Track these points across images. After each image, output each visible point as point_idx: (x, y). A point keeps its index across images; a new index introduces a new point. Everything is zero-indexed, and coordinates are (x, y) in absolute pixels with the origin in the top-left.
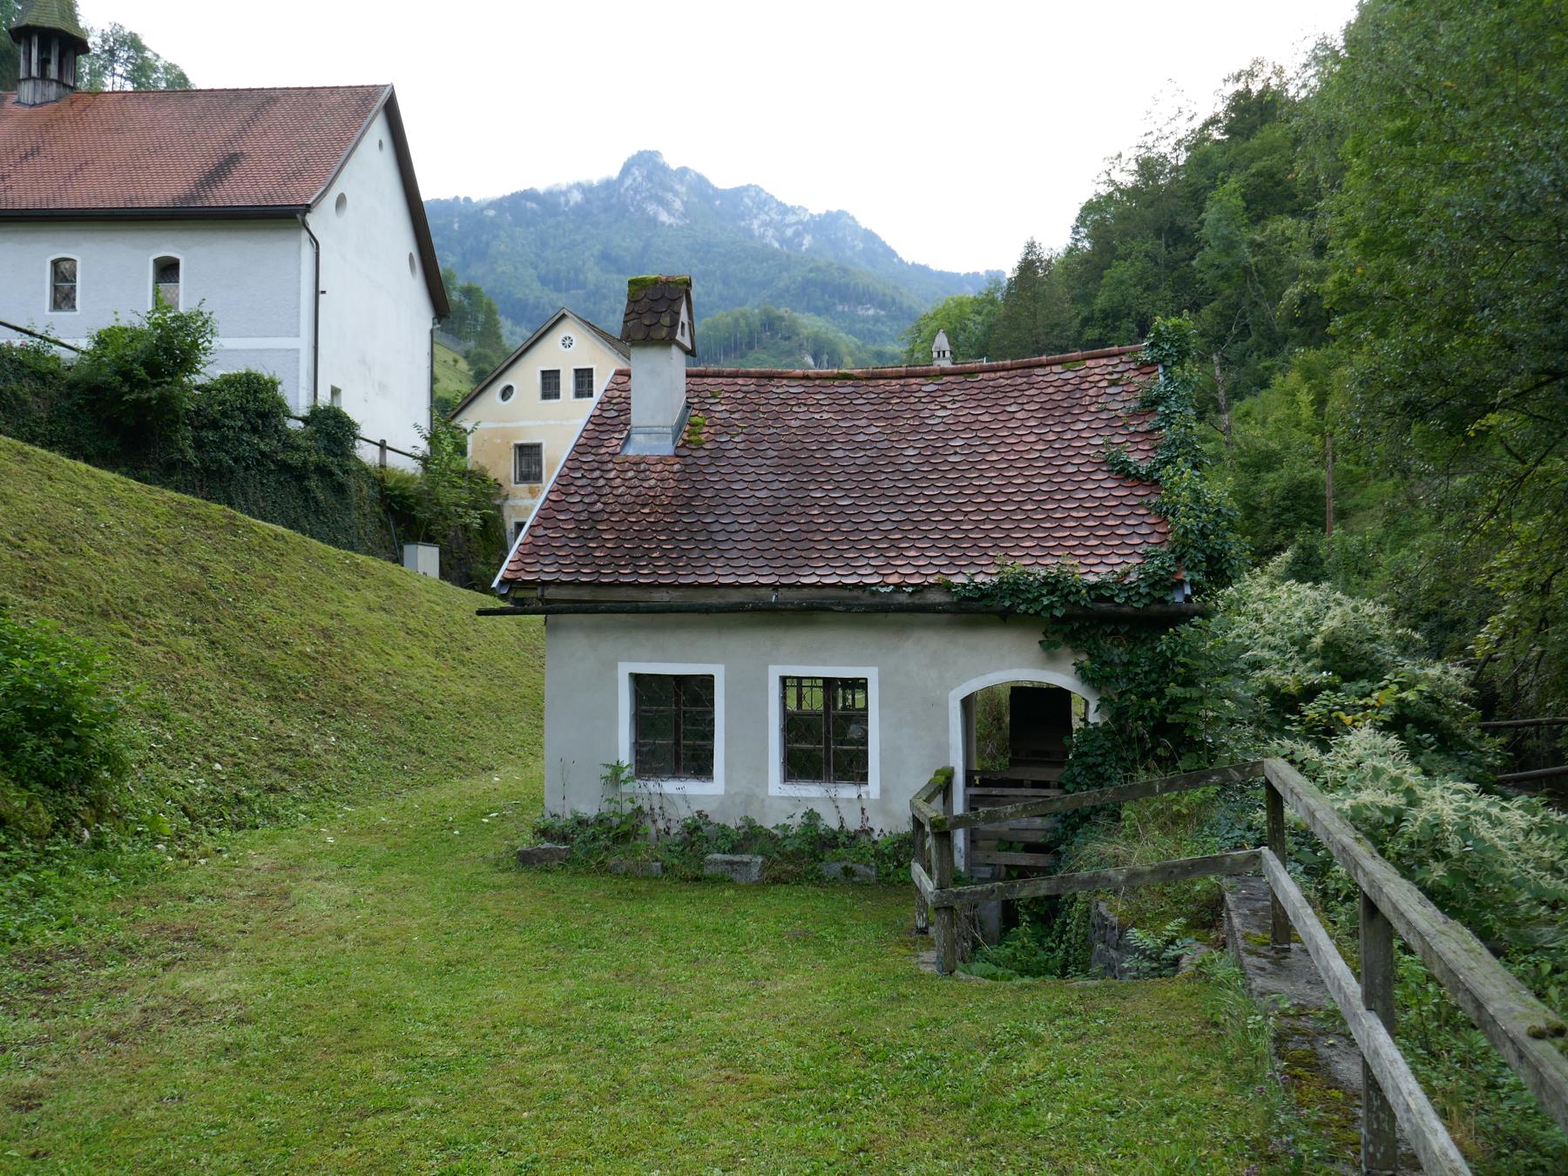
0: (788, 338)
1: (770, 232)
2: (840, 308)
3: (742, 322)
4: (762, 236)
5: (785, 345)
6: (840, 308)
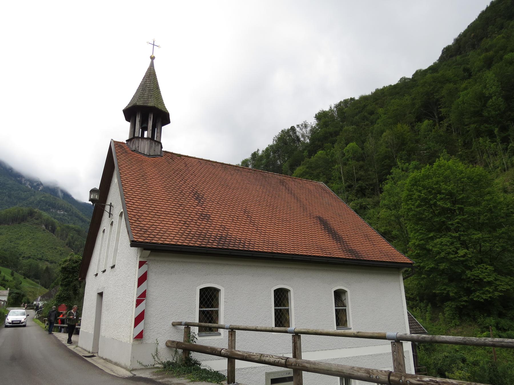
0: (37, 219)
1: (28, 183)
2: (52, 210)
3: (21, 212)
4: (25, 184)
5: (36, 221)
6: (52, 210)
